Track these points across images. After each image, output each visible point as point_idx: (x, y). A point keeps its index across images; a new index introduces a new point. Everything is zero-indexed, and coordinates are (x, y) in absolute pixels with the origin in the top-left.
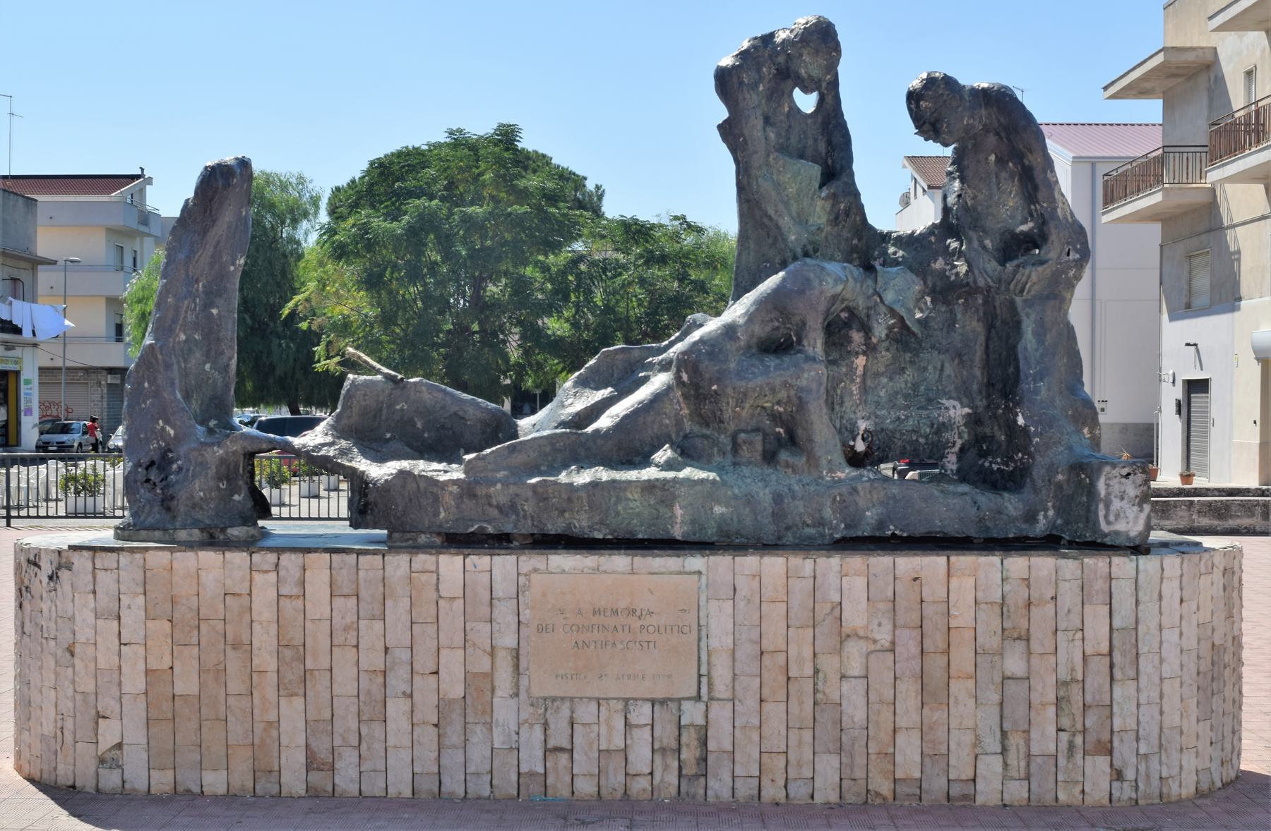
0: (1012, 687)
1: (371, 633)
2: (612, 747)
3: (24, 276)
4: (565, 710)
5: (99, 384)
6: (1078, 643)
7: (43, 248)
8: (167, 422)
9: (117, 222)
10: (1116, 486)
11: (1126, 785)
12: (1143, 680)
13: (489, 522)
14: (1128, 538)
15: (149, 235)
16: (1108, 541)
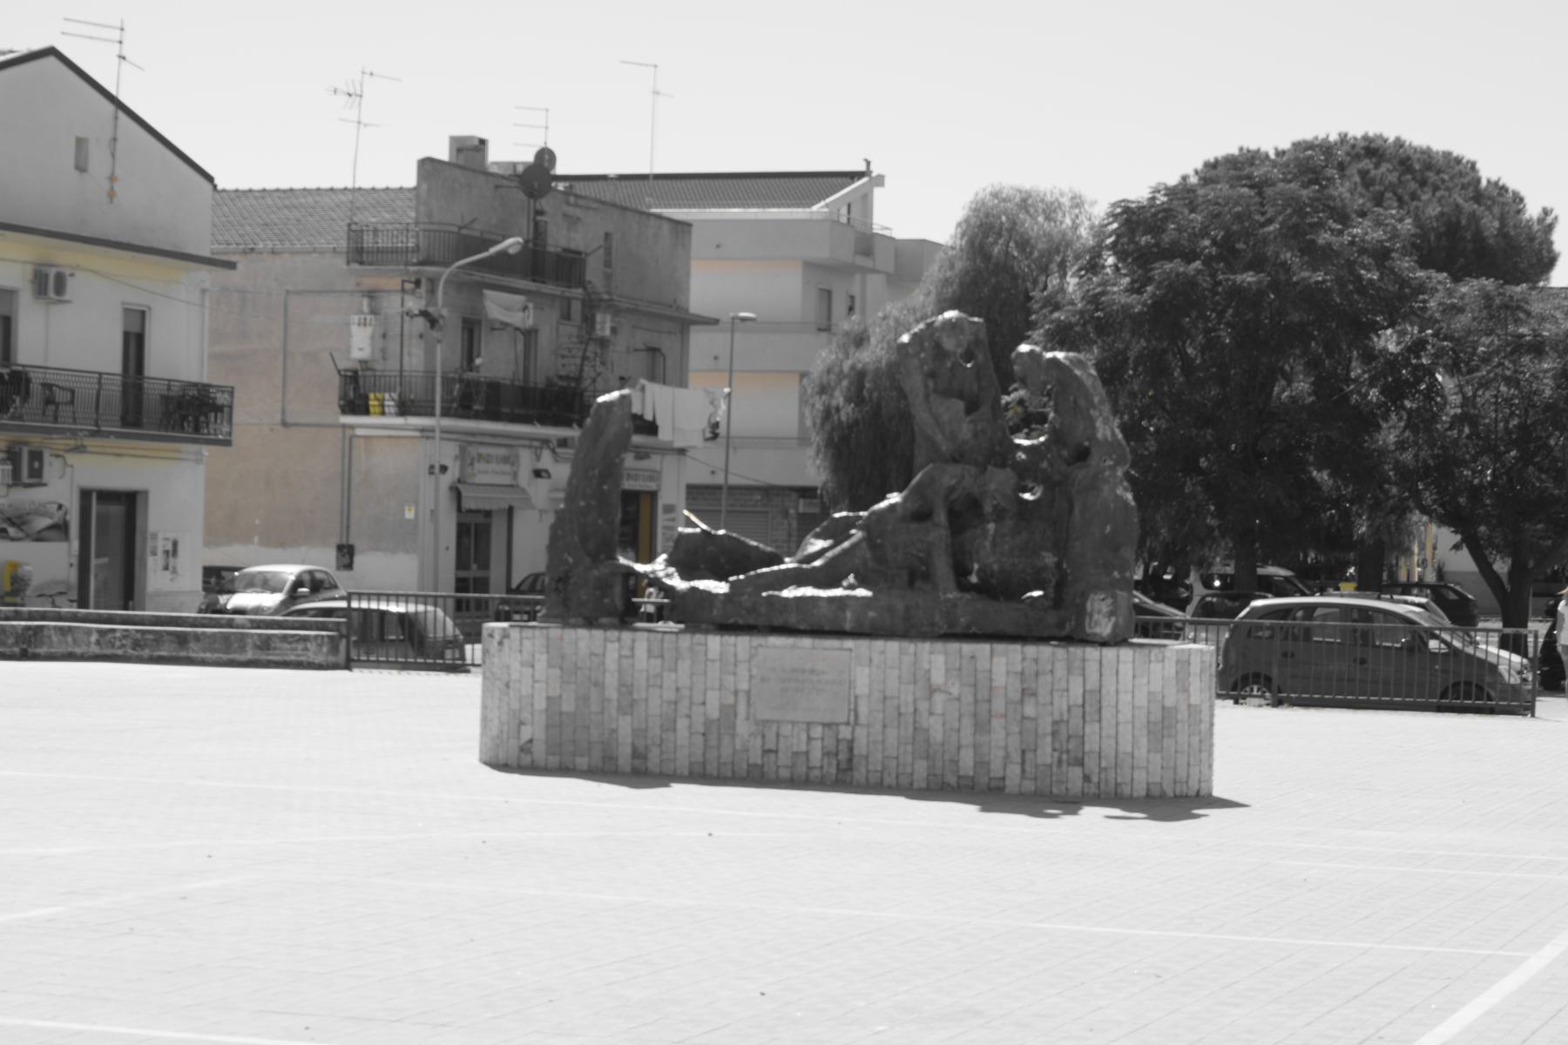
0: (1028, 724)
1: (669, 679)
3: (668, 344)
4: (774, 728)
5: (786, 514)
10: (1097, 606)
12: (1104, 722)
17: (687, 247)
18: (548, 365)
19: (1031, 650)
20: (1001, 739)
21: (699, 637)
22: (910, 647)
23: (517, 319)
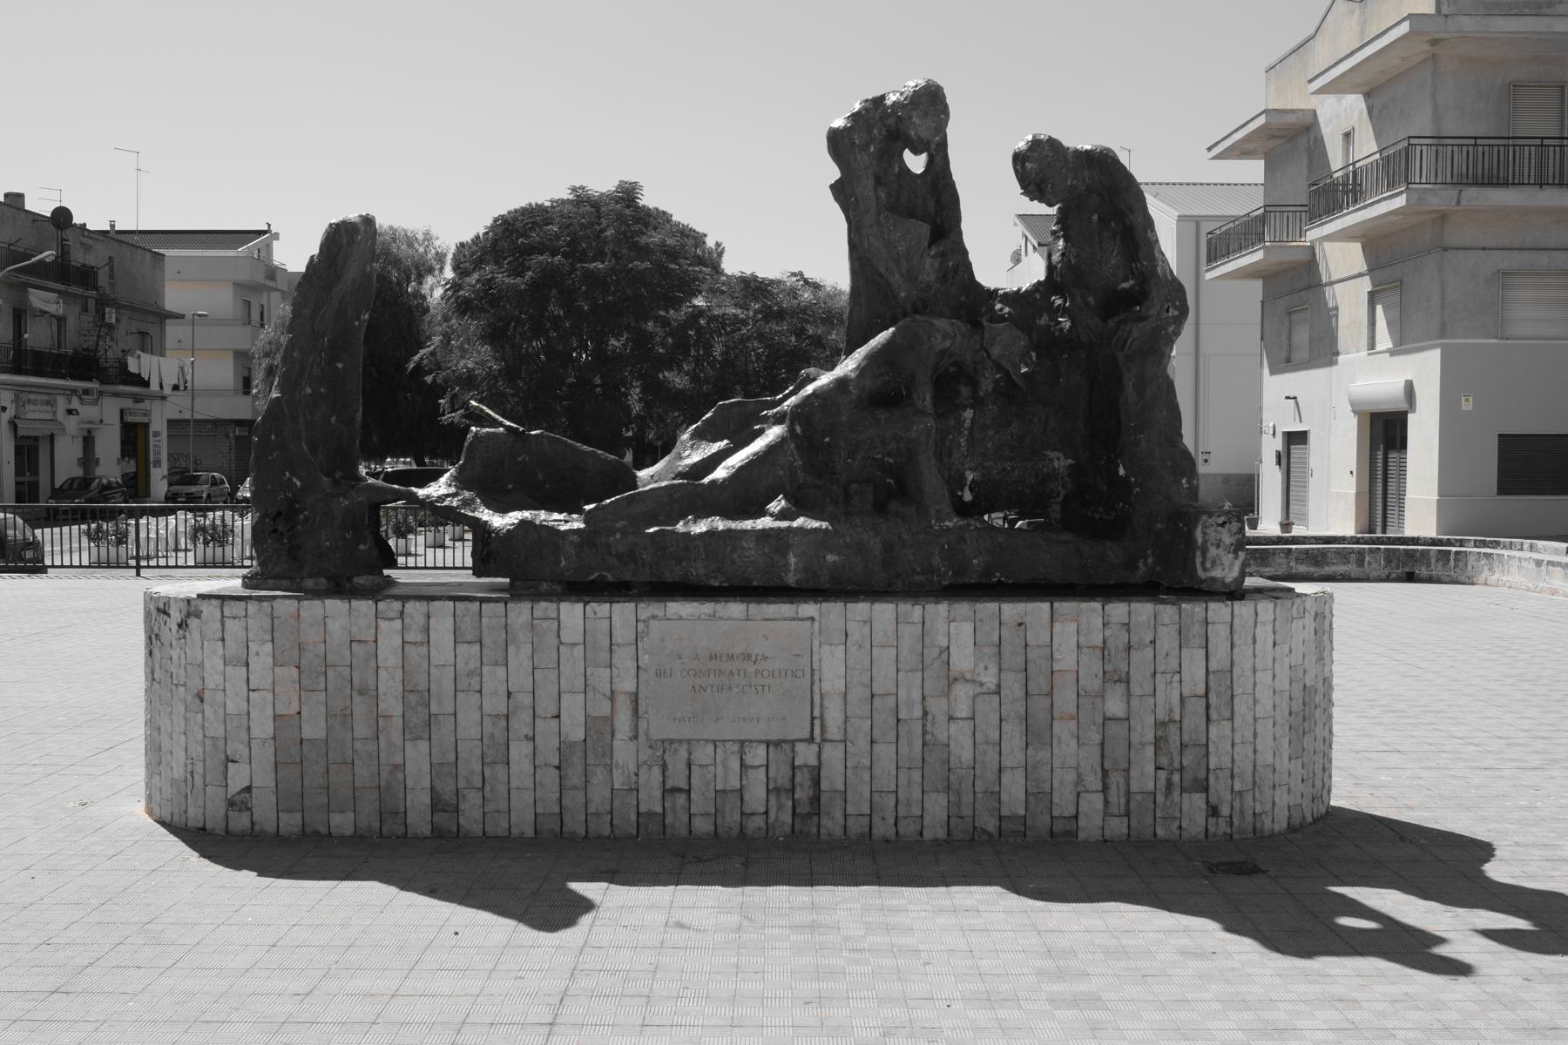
0: (1113, 728)
1: (494, 678)
3: (153, 330)
4: (683, 753)
5: (227, 436)
6: (1176, 685)
8: (293, 474)
9: (244, 276)
11: (1221, 820)
12: (1238, 719)
16: (1204, 587)
17: (162, 269)
18: (74, 340)
19: (1118, 610)
20: (1071, 754)
21: (544, 607)
22: (914, 611)
23: (52, 308)
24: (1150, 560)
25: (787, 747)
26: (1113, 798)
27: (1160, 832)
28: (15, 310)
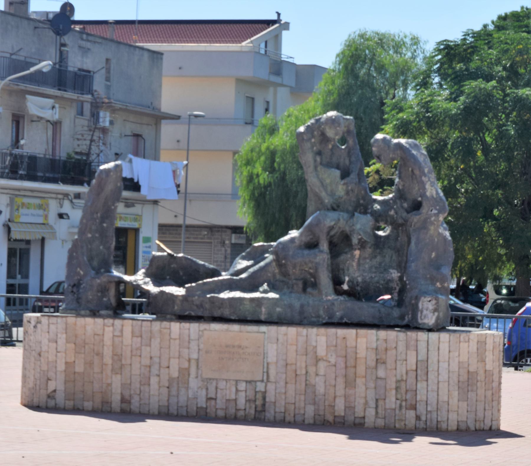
0: (380, 382)
1: (146, 351)
2: (230, 398)
3: (147, 132)
5: (223, 243)
6: (404, 365)
7: (168, 103)
8: (81, 269)
9: (247, 73)
11: (421, 422)
12: (430, 381)
13: (193, 311)
14: (428, 326)
15: (282, 85)
16: (421, 326)
18: (68, 147)
21: (165, 324)
23: (48, 114)
24: (410, 316)
25: (253, 383)
26: (380, 411)
27: (397, 426)
28: (14, 115)
